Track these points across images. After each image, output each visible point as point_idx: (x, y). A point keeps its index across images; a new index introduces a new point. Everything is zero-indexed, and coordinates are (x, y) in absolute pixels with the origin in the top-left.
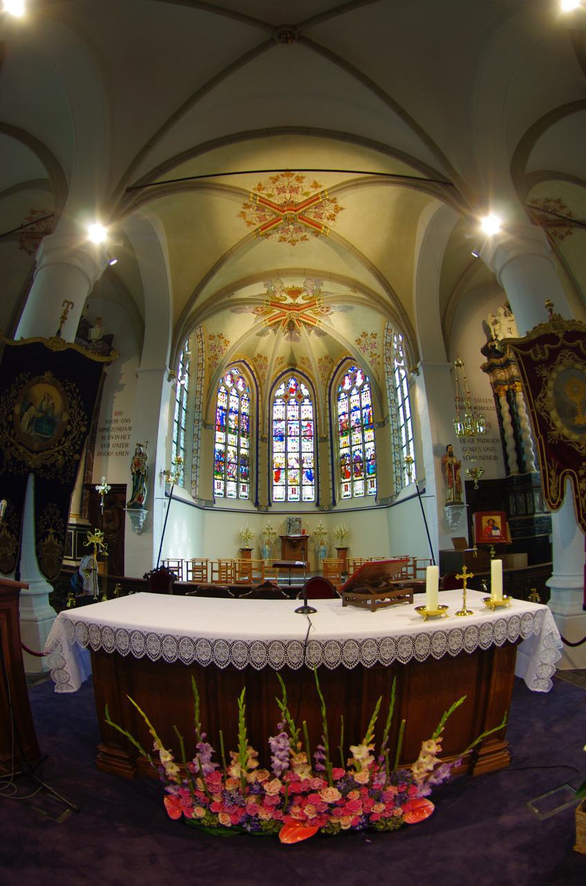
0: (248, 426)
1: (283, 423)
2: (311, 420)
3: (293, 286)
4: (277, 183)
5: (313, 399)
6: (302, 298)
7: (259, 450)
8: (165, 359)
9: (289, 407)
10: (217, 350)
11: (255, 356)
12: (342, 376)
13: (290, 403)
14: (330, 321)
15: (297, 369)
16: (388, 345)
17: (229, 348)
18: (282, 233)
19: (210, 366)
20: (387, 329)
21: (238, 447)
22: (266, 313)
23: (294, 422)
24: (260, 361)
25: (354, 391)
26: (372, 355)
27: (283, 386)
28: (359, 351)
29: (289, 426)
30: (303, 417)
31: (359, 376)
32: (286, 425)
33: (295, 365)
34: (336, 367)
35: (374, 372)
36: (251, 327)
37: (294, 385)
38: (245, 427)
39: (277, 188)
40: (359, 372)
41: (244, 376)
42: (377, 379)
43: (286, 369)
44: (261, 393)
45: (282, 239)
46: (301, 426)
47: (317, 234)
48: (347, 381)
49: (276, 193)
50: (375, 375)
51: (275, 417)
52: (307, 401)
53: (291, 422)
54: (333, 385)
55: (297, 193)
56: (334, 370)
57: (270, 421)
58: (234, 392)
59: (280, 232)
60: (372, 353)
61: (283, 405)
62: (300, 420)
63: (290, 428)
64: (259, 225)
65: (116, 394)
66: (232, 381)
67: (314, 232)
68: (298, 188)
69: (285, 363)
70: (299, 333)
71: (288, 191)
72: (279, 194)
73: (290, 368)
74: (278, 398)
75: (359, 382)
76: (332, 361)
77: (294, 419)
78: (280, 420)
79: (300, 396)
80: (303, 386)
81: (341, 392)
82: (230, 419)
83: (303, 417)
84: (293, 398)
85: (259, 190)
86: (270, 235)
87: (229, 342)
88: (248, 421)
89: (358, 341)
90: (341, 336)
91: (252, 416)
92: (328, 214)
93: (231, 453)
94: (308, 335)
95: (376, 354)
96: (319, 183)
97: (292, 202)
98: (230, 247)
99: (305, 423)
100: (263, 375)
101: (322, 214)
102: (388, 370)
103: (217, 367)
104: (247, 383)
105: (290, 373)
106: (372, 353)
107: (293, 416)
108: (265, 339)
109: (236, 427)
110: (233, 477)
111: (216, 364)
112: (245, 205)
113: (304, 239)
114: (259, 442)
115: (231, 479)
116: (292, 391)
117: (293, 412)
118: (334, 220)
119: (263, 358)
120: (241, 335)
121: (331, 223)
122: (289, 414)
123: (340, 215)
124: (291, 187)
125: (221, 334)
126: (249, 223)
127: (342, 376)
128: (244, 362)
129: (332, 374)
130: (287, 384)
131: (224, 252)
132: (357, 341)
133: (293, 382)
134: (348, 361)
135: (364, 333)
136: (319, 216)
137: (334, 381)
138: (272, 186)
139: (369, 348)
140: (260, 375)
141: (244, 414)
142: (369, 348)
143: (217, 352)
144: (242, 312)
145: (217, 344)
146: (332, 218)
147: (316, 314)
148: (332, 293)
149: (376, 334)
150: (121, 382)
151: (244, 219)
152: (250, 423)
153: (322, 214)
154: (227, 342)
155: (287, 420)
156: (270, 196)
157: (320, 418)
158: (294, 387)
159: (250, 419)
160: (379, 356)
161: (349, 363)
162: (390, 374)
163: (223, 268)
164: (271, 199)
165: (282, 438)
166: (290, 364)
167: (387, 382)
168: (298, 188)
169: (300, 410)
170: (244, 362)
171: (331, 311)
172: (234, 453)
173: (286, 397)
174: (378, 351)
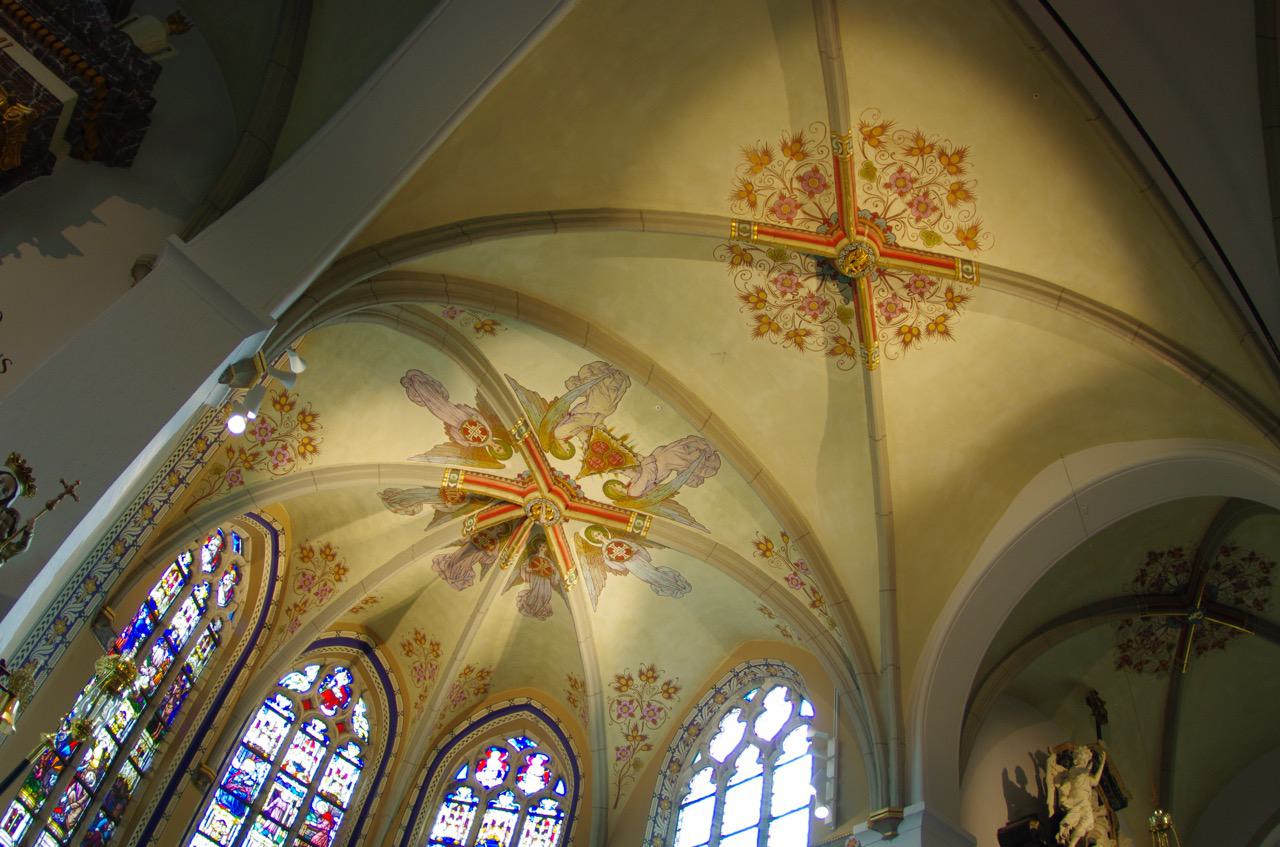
0: (176, 709)
1: (264, 769)
2: (340, 807)
3: (625, 438)
4: (912, 160)
5: (377, 763)
6: (605, 486)
7: (174, 798)
8: (281, 300)
9: (300, 738)
10: (270, 446)
11: (316, 544)
12: (487, 742)
13: (309, 729)
14: (598, 588)
15: (378, 653)
16: (693, 730)
17: (304, 466)
18: (775, 281)
19: (217, 471)
20: (718, 691)
21: (123, 748)
22: (479, 455)
23: (294, 783)
24: (314, 568)
25: (506, 800)
26: (635, 735)
27: (313, 671)
28: (606, 706)
29: (277, 786)
30: (325, 786)
31: (536, 768)
32: (270, 779)
33: (380, 641)
34: (483, 713)
35: (613, 778)
36: (404, 460)
37: (344, 689)
38: (169, 710)
39: (901, 170)
40: (539, 760)
41: (247, 572)
42: (611, 806)
43: (352, 635)
44: (262, 649)
45: (755, 299)
46: (306, 808)
47: (838, 348)
48: (494, 761)
49: (886, 179)
50: (613, 789)
51: (251, 736)
52: (353, 752)
53: (286, 779)
54: (453, 752)
55: (918, 219)
56: (475, 718)
57: (231, 739)
58: (202, 593)
59: (774, 275)
60: (636, 728)
61: (288, 719)
62: (312, 787)
63: (277, 794)
64: (760, 215)
65: (24, 248)
66: (216, 561)
67: (836, 339)
68: (935, 209)
69: (360, 618)
70: (485, 567)
71: (909, 197)
72: (887, 186)
73: (363, 638)
74: (288, 694)
75: (532, 782)
76: (484, 690)
77: (300, 776)
78: (258, 755)
79: (344, 726)
80: (360, 708)
81: (462, 783)
82: (151, 658)
83: (325, 786)
84: (323, 719)
85: (869, 137)
86: (750, 263)
87: (315, 450)
88: (183, 697)
89: (623, 682)
90: (593, 644)
91: (203, 694)
92: (909, 322)
93: (98, 752)
94: (501, 591)
95: (644, 738)
96: (979, 238)
97: (889, 229)
98: (646, 206)
99: (321, 807)
100: (301, 608)
101: (903, 310)
102: (665, 794)
103: (237, 489)
104: (242, 596)
105: (353, 651)
106: (636, 728)
107: (300, 768)
108: (390, 519)
109: (150, 688)
110: (63, 826)
111: (236, 479)
112: (798, 141)
113: (797, 338)
114: (187, 777)
115: (55, 828)
116: (329, 699)
117: (303, 756)
118: (906, 344)
119: (332, 565)
120: (363, 461)
121: (895, 347)
122: (293, 755)
123: (929, 344)
124: (926, 195)
125: (314, 416)
126: (747, 193)
127: (487, 742)
128: (275, 535)
129: (465, 725)
130: (326, 675)
131: (613, 204)
132: (619, 678)
133: (342, 679)
134: (526, 714)
135: (652, 669)
136: (891, 309)
137: (458, 746)
138: (899, 156)
139: (638, 713)
140: (290, 601)
141: (188, 669)
142: (638, 713)
143: (263, 450)
144: (424, 403)
145: (282, 430)
146: (908, 336)
147: (587, 547)
148: (692, 522)
149: (676, 690)
150: (70, 233)
151: (753, 171)
152: (187, 707)
153: (903, 310)
154: (310, 447)
155: (277, 767)
156: (869, 172)
157: (378, 818)
158: (339, 694)
159: (194, 696)
160: (649, 747)
161: (524, 724)
162: (665, 804)
163: (569, 240)
164: (860, 183)
165: (240, 804)
166: (368, 629)
167: (650, 823)
168: (935, 209)
169: (325, 761)
170: (275, 535)
171: (628, 565)
172: (104, 760)
173: (308, 704)
174: (655, 734)
